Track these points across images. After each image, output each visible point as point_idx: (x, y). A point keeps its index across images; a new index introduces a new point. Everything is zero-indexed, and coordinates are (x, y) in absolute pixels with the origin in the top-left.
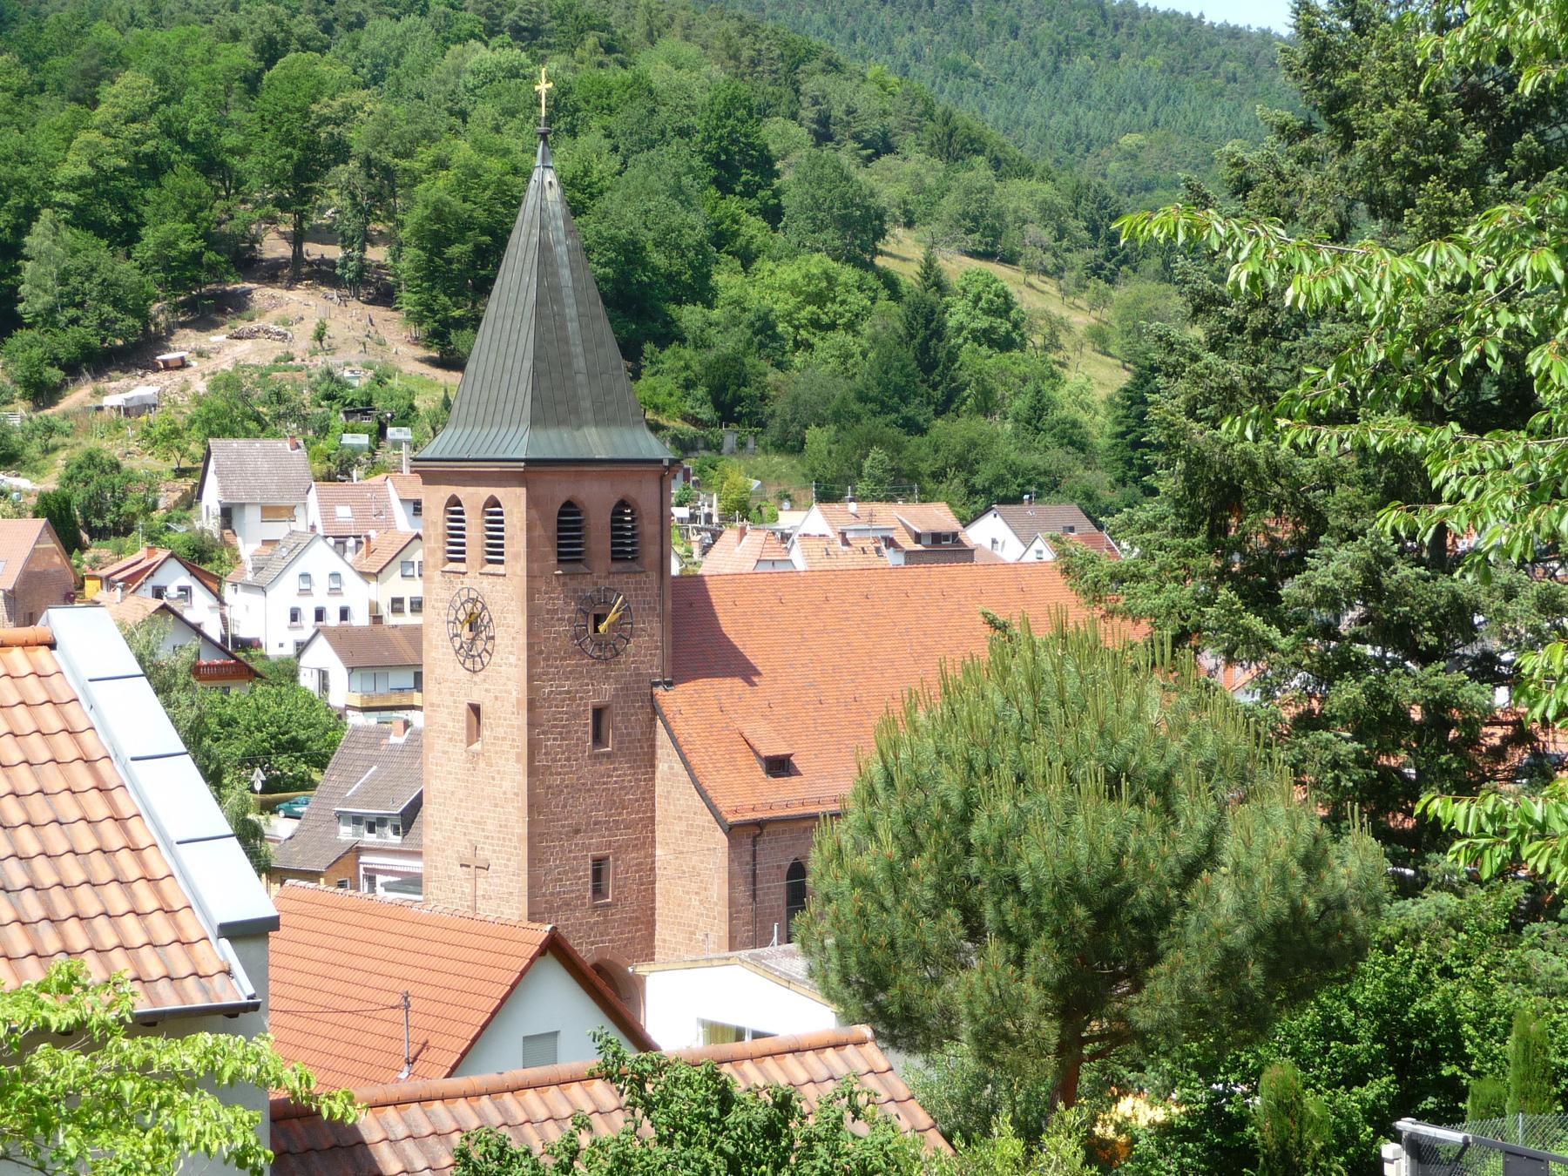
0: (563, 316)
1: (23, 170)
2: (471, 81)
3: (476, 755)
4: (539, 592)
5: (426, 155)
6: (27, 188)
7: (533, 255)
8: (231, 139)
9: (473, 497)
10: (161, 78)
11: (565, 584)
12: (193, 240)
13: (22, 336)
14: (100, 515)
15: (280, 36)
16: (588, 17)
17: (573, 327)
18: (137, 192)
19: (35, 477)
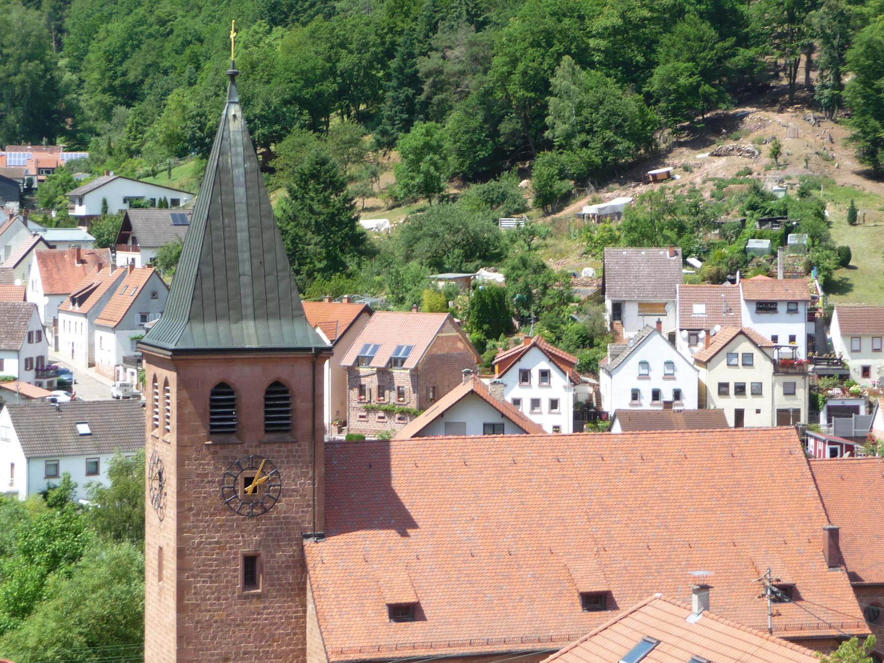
4: (189, 459)
11: (215, 453)
12: (690, 76)
13: (546, 156)
17: (242, 236)
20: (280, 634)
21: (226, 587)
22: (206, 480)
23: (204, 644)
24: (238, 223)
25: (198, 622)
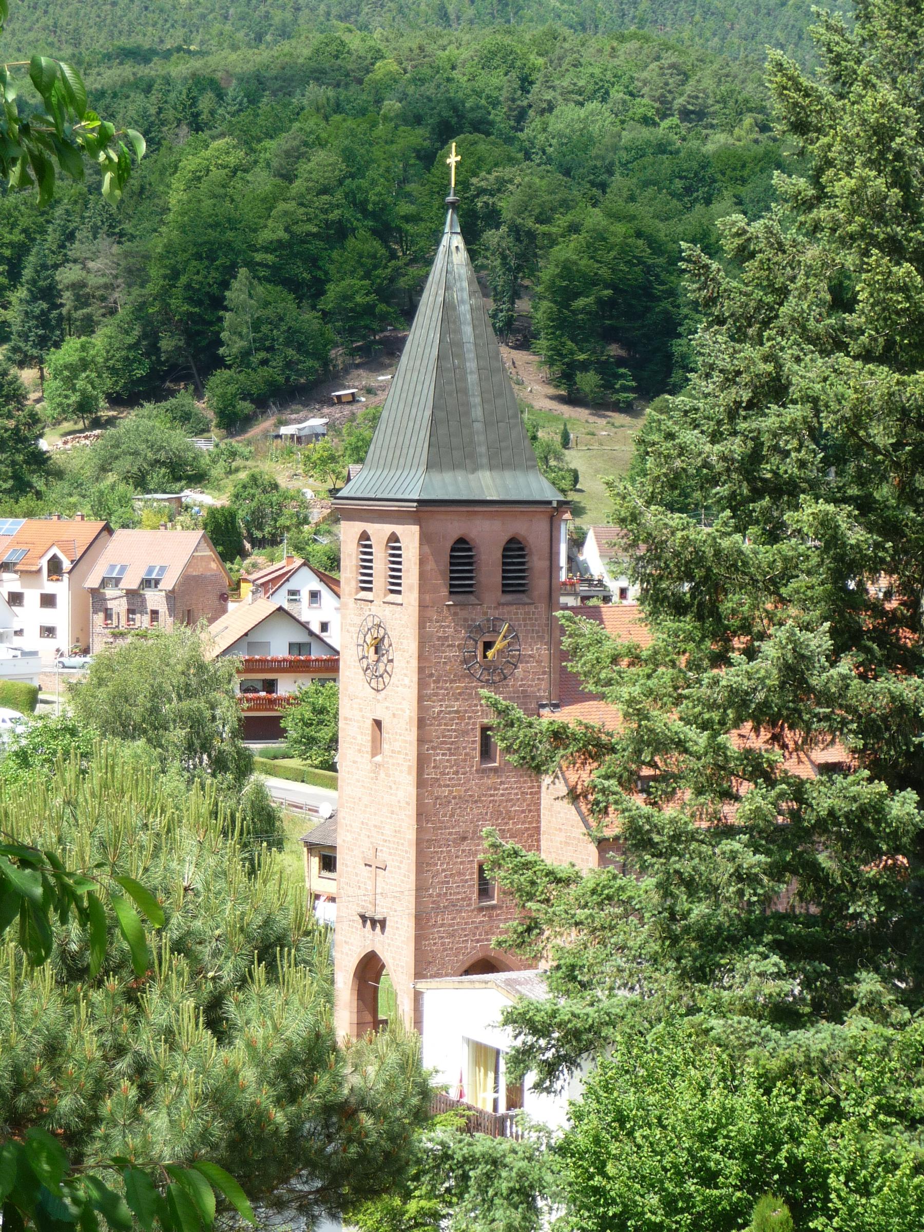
0: (464, 370)
1: (230, 235)
2: (624, 155)
3: (378, 765)
4: (431, 621)
5: (562, 221)
6: (233, 250)
7: (438, 315)
8: (405, 208)
9: (380, 531)
10: (348, 156)
11: (455, 614)
12: (367, 294)
13: (222, 375)
14: (260, 528)
15: (454, 121)
16: (746, 101)
17: (472, 379)
18: (324, 254)
19: (216, 494)
21: (465, 760)
24: (468, 364)
25: (437, 798)
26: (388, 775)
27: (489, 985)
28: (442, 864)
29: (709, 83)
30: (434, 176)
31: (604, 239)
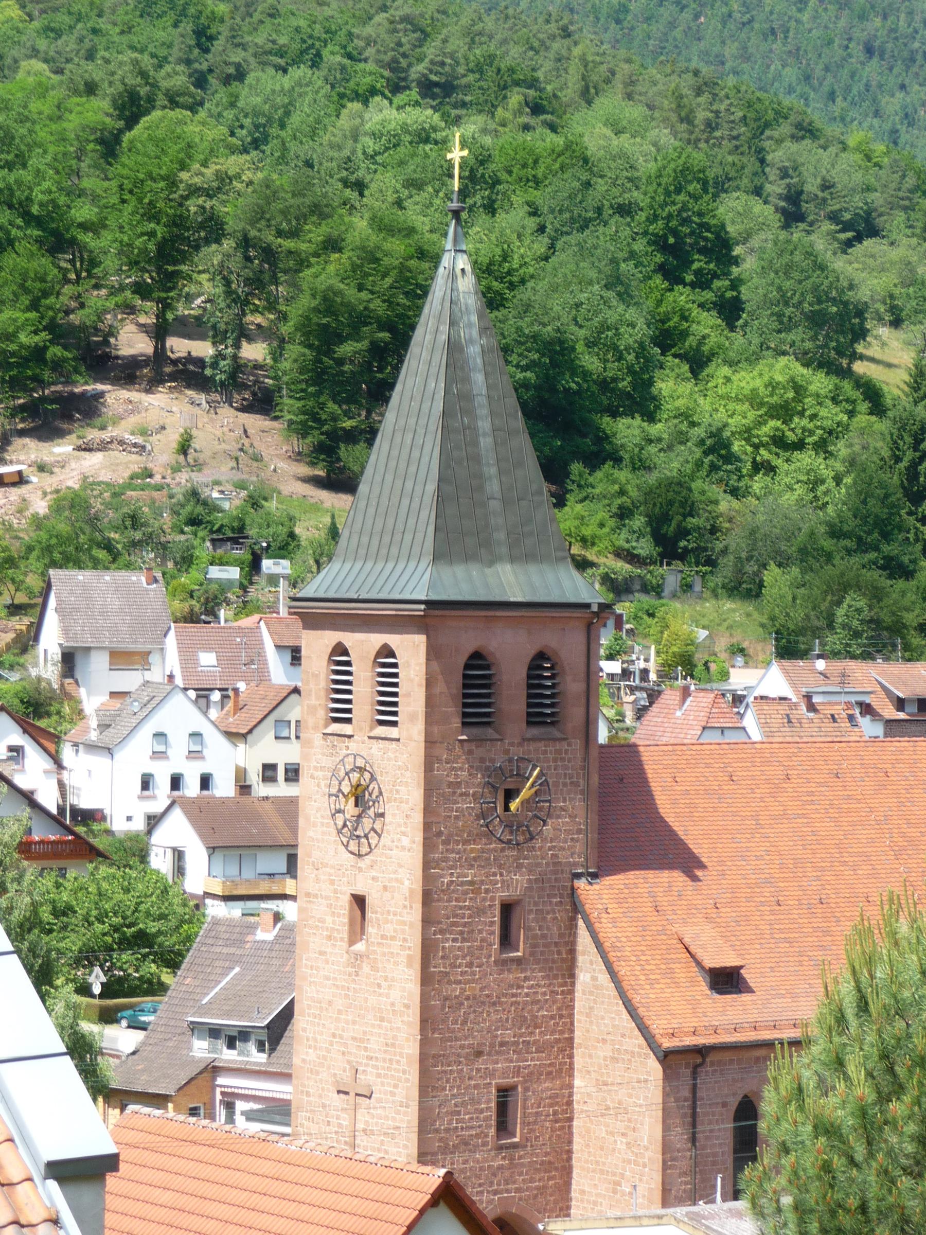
0: (475, 430)
2: (370, 144)
3: (359, 956)
4: (439, 761)
5: (316, 233)
7: (440, 358)
11: (470, 752)
12: (36, 332)
15: (143, 91)
16: (512, 70)
17: (486, 442)
20: (543, 1016)
21: (481, 948)
22: (459, 791)
23: (453, 1031)
24: (480, 423)
25: (446, 999)
26: (374, 968)
27: (664, 1220)
28: (452, 1088)
29: (457, 44)
30: (124, 166)
31: (377, 260)
